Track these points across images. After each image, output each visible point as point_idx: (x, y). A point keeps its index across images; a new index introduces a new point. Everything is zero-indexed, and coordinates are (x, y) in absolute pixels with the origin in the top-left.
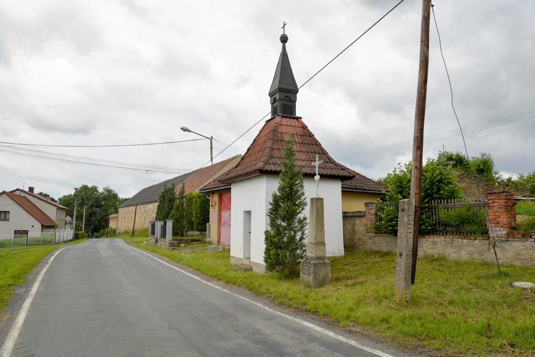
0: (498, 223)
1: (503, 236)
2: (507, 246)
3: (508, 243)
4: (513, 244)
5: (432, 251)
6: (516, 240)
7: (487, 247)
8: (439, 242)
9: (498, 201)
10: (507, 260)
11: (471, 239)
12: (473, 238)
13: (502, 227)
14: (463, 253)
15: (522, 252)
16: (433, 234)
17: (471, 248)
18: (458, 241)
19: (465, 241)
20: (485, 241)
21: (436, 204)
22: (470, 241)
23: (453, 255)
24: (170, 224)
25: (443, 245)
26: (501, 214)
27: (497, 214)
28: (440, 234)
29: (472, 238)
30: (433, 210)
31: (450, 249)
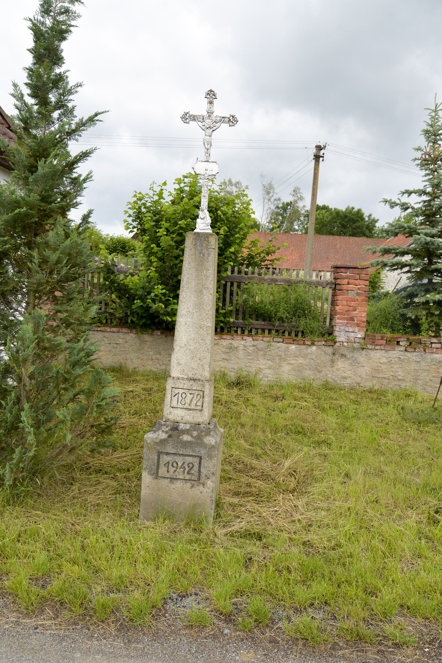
0: (352, 319)
1: (357, 340)
2: (361, 357)
3: (364, 352)
4: (372, 353)
5: (223, 364)
6: (378, 347)
7: (328, 358)
8: (242, 347)
9: (357, 282)
10: (358, 380)
11: (304, 344)
12: (309, 343)
13: (358, 325)
14: (286, 368)
15: (384, 367)
16: (243, 332)
17: (301, 360)
18: (280, 346)
19: (293, 347)
20: (327, 348)
21: (236, 274)
22: (303, 347)
23: (267, 371)
24: (37, 341)
25: (249, 354)
26: (359, 305)
27: (353, 304)
28: (236, 332)
29: (307, 343)
30: (229, 284)
31: (262, 361)
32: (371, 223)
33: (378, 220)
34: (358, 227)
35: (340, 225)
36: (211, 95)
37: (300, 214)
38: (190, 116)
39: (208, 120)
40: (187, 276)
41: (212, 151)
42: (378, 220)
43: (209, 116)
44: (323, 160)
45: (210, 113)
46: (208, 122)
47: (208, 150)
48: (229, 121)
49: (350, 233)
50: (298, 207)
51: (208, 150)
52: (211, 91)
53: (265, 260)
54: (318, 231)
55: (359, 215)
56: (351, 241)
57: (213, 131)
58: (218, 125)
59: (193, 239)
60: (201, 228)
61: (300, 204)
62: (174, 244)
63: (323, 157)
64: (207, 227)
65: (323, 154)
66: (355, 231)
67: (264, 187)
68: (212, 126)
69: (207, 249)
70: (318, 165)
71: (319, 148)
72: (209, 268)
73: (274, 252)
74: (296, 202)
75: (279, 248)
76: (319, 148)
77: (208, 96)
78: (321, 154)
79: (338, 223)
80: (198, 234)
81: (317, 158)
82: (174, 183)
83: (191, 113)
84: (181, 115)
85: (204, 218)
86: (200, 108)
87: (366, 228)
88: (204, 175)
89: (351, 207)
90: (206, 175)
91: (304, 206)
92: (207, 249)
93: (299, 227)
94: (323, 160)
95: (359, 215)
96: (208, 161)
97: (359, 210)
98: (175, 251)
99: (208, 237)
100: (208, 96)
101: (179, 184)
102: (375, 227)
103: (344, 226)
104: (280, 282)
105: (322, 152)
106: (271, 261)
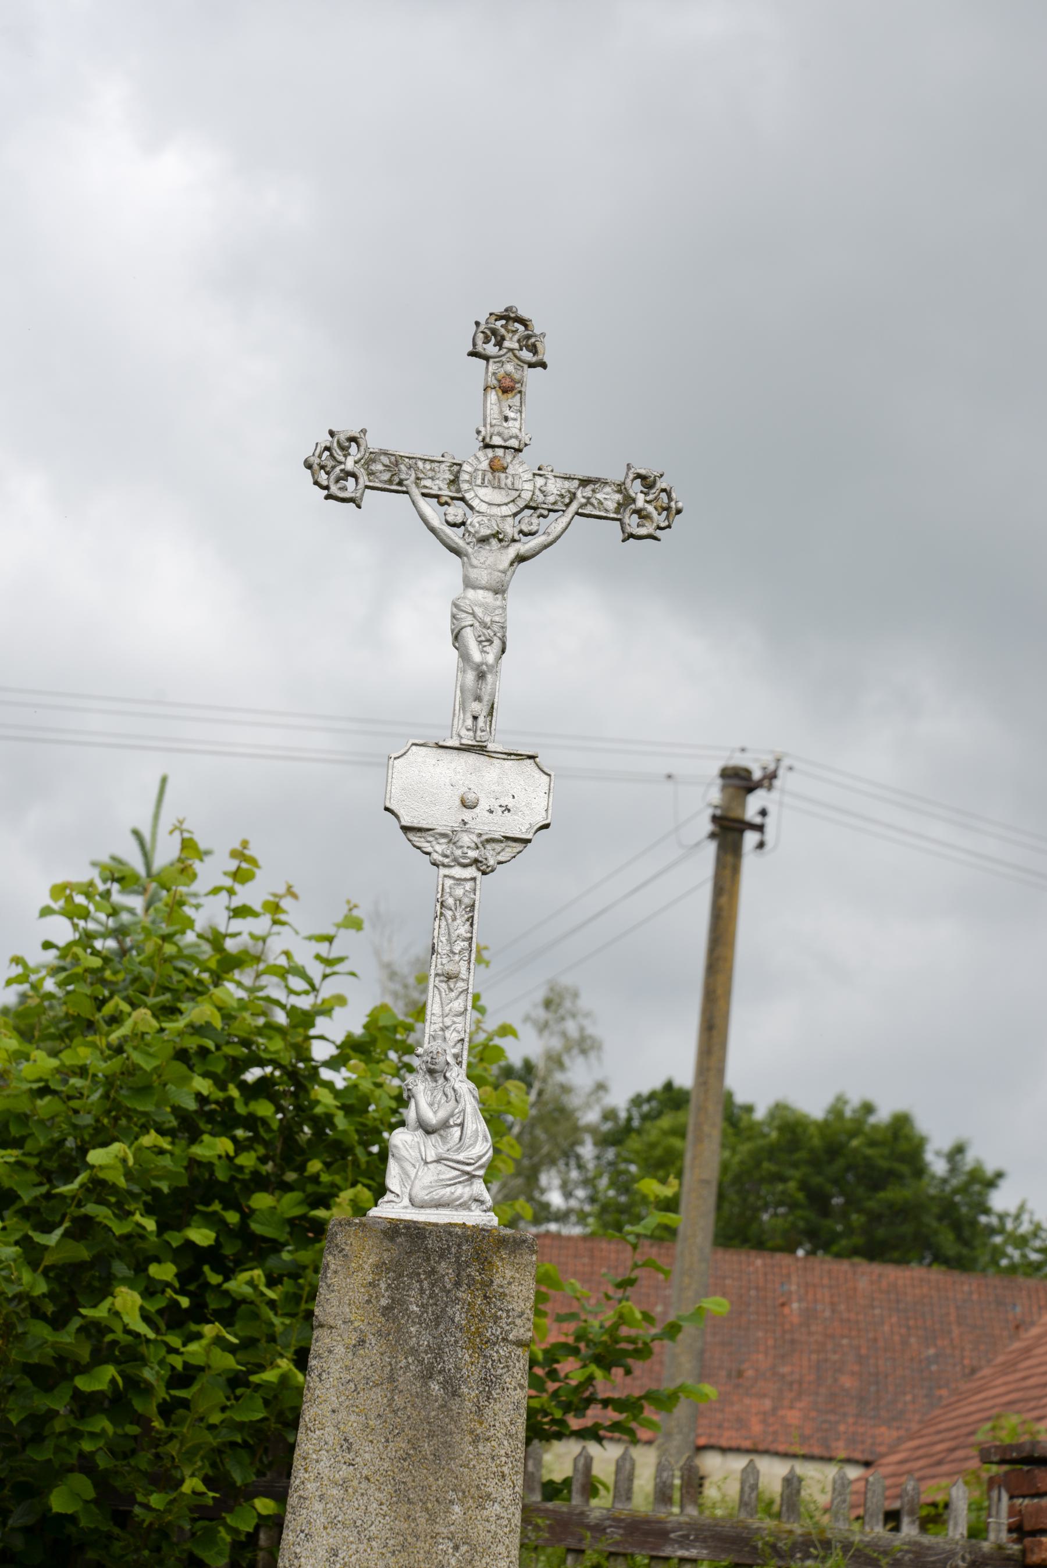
32: (964, 1189)
33: (1000, 1175)
34: (904, 1212)
35: (800, 1196)
36: (508, 340)
37: (576, 1129)
38: (371, 458)
39: (487, 493)
40: (324, 1541)
41: (509, 684)
42: (1000, 1175)
43: (496, 468)
44: (761, 845)
45: (500, 453)
46: (489, 504)
47: (481, 676)
48: (620, 507)
49: (858, 1240)
50: (566, 1089)
51: (481, 676)
52: (509, 317)
53: (590, 1401)
54: (736, 1232)
55: (901, 1141)
56: (863, 1283)
57: (521, 559)
58: (556, 524)
59: (380, 1268)
60: (421, 1195)
61: (579, 1075)
62: (42, 1287)
63: (760, 828)
64: (463, 1191)
65: (763, 813)
66: (881, 1232)
67: (393, 975)
68: (510, 528)
69: (480, 1344)
70: (736, 870)
71: (739, 781)
72: (491, 1487)
73: (643, 1352)
74: (556, 1061)
75: (673, 1330)
76: (739, 781)
77: (491, 349)
78: (751, 813)
79: (792, 1185)
80: (411, 1234)
81: (729, 830)
82: (46, 912)
83: (373, 442)
84: (307, 452)
85: (445, 1125)
86: (438, 412)
87: (940, 1218)
88: (450, 838)
89: (855, 1100)
90: (466, 839)
91: (601, 1087)
92: (480, 1344)
93: (568, 1195)
94: (761, 845)
95: (903, 1146)
96: (480, 749)
97: (901, 1123)
98: (41, 1330)
99: (485, 1263)
100: (491, 349)
101: (74, 913)
102: (987, 1211)
103: (818, 1200)
104: (684, 1542)
105: (754, 803)
106: (619, 1405)
